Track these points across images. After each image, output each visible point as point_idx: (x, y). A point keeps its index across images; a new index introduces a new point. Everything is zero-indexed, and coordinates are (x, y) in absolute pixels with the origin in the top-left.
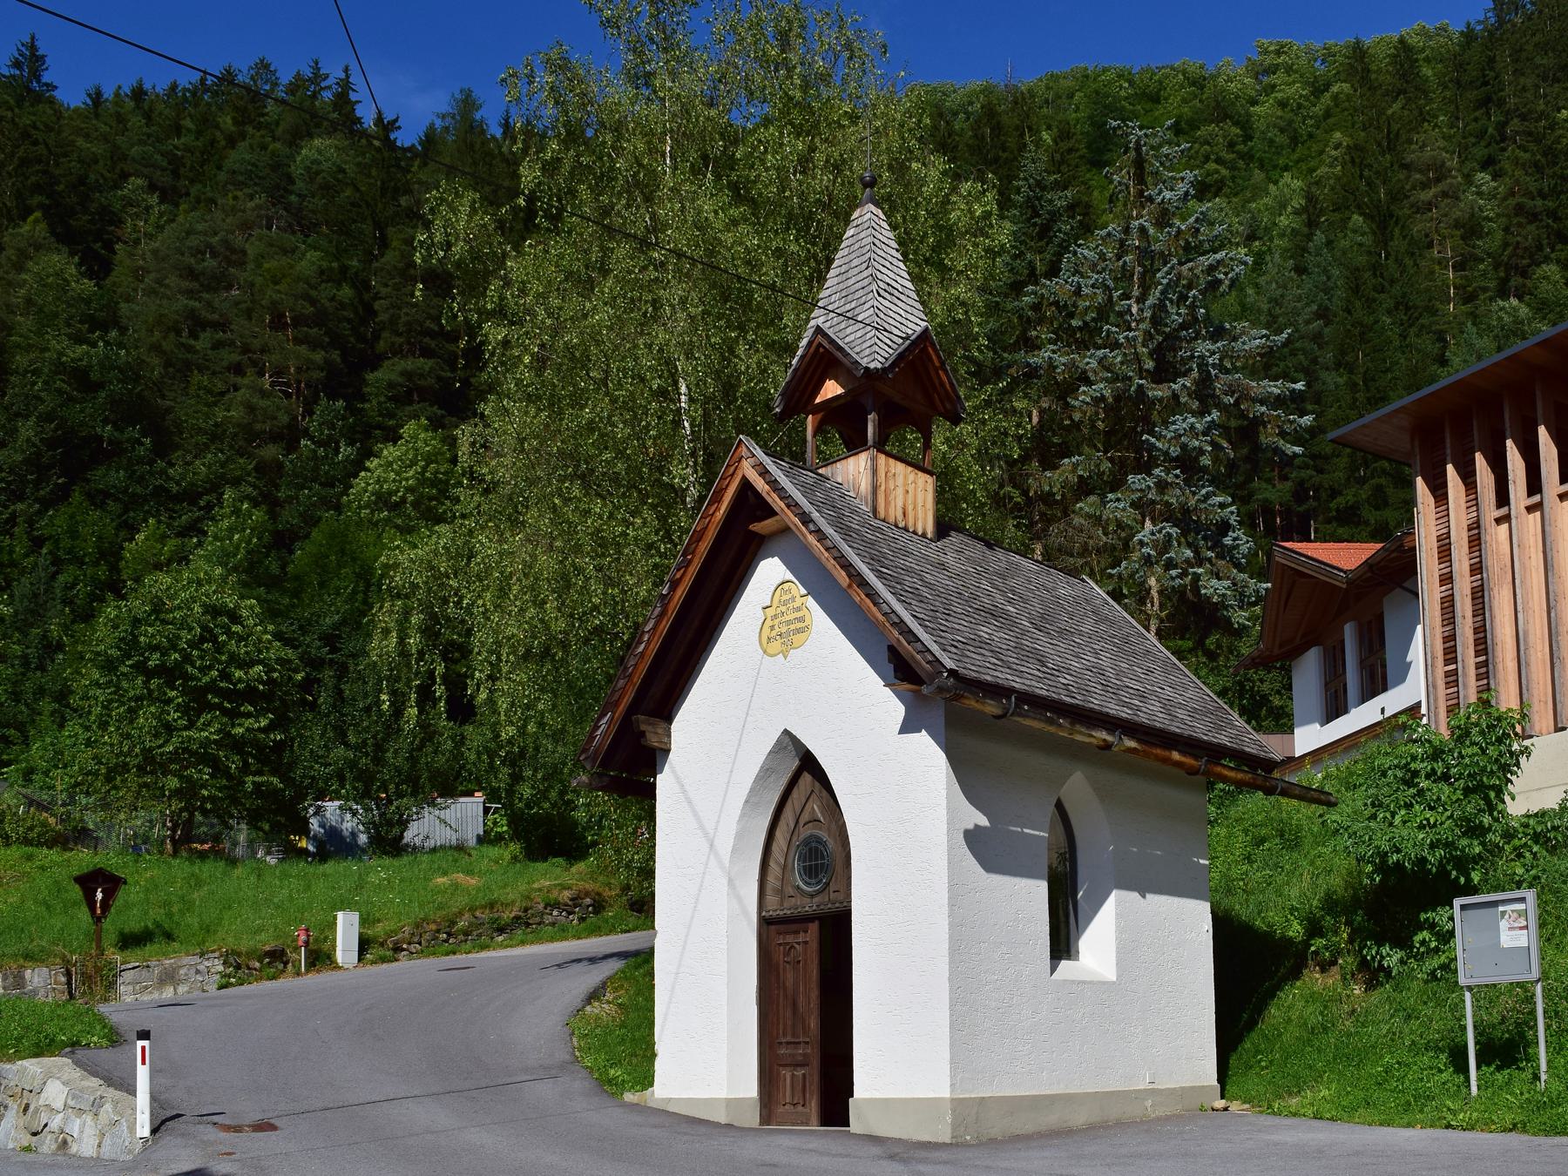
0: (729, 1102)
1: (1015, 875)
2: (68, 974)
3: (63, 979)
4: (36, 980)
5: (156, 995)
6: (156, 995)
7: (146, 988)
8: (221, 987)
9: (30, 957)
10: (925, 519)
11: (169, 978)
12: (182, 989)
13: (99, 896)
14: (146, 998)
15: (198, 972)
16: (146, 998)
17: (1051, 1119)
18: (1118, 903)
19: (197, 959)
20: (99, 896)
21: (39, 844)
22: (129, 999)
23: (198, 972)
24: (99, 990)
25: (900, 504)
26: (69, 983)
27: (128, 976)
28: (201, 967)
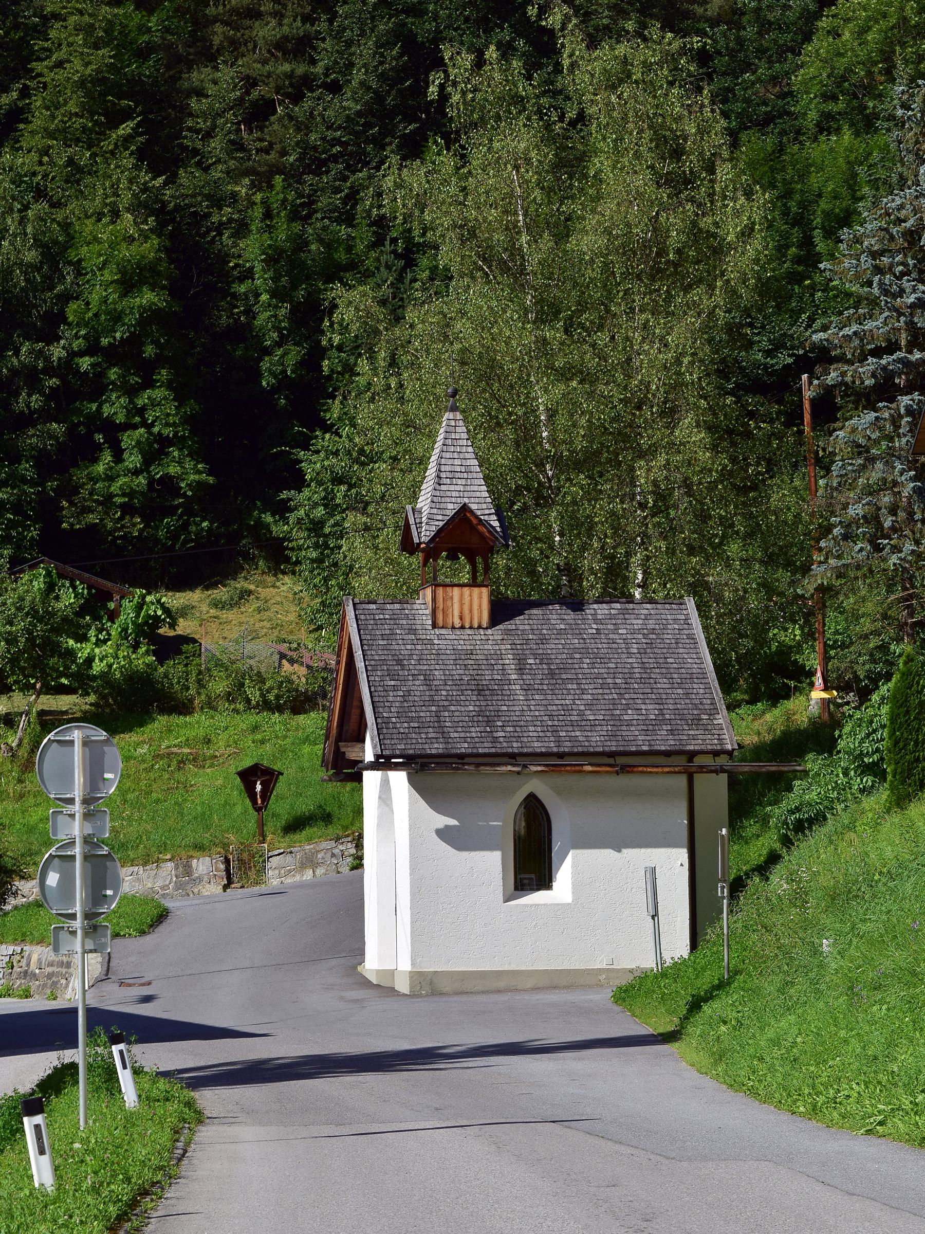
0: (378, 971)
1: (475, 849)
2: (227, 861)
3: (222, 867)
4: (201, 868)
5: (298, 878)
6: (298, 878)
7: (290, 871)
8: (352, 869)
9: (200, 847)
10: (480, 617)
11: (310, 862)
12: (320, 871)
13: (259, 787)
14: (289, 880)
15: (333, 855)
16: (289, 880)
17: (502, 984)
18: (574, 865)
19: (333, 844)
20: (259, 787)
21: (280, 709)
22: (275, 882)
23: (333, 855)
24: (252, 874)
25: (456, 613)
26: (227, 870)
27: (275, 861)
28: (336, 851)
